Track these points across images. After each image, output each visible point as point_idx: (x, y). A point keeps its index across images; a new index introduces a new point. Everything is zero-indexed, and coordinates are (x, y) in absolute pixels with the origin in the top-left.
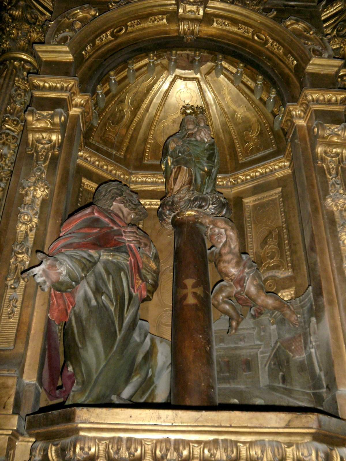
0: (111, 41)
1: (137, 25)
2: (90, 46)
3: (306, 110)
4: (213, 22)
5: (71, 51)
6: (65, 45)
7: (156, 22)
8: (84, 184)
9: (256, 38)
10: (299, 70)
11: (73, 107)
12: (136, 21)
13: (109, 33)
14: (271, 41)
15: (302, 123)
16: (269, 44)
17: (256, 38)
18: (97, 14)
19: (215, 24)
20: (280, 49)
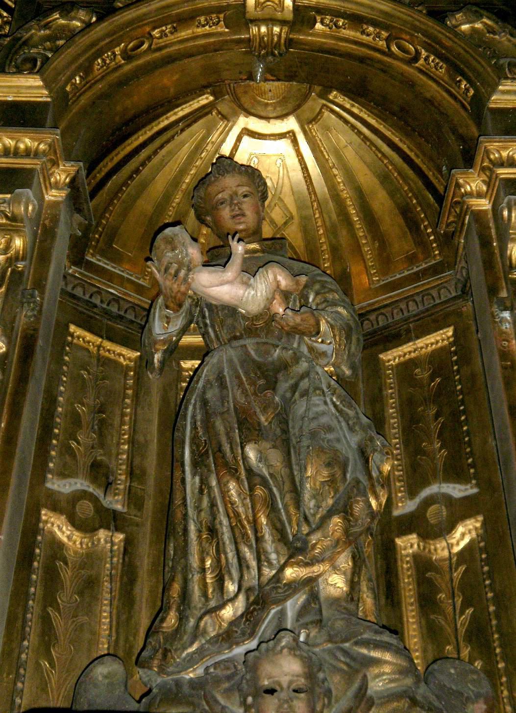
0: (482, 162)
1: (172, 33)
2: (80, 76)
3: (490, 178)
4: (315, 22)
5: (47, 85)
6: (31, 72)
7: (207, 27)
8: (72, 335)
9: (394, 48)
10: (478, 106)
11: (51, 188)
12: (169, 26)
13: (117, 51)
14: (424, 53)
15: (484, 204)
16: (422, 61)
17: (394, 48)
18: (94, 19)
19: (318, 26)
20: (441, 68)
